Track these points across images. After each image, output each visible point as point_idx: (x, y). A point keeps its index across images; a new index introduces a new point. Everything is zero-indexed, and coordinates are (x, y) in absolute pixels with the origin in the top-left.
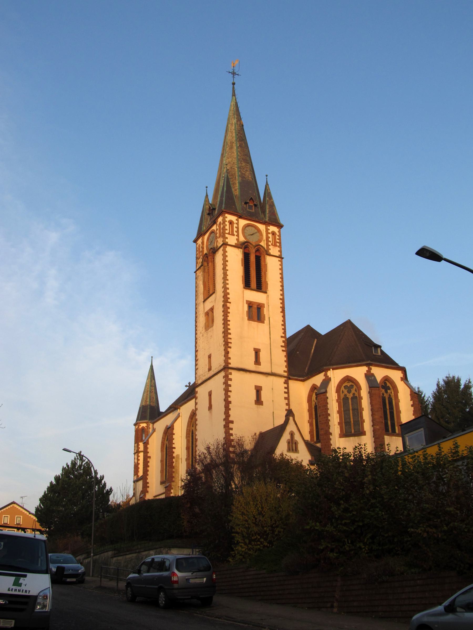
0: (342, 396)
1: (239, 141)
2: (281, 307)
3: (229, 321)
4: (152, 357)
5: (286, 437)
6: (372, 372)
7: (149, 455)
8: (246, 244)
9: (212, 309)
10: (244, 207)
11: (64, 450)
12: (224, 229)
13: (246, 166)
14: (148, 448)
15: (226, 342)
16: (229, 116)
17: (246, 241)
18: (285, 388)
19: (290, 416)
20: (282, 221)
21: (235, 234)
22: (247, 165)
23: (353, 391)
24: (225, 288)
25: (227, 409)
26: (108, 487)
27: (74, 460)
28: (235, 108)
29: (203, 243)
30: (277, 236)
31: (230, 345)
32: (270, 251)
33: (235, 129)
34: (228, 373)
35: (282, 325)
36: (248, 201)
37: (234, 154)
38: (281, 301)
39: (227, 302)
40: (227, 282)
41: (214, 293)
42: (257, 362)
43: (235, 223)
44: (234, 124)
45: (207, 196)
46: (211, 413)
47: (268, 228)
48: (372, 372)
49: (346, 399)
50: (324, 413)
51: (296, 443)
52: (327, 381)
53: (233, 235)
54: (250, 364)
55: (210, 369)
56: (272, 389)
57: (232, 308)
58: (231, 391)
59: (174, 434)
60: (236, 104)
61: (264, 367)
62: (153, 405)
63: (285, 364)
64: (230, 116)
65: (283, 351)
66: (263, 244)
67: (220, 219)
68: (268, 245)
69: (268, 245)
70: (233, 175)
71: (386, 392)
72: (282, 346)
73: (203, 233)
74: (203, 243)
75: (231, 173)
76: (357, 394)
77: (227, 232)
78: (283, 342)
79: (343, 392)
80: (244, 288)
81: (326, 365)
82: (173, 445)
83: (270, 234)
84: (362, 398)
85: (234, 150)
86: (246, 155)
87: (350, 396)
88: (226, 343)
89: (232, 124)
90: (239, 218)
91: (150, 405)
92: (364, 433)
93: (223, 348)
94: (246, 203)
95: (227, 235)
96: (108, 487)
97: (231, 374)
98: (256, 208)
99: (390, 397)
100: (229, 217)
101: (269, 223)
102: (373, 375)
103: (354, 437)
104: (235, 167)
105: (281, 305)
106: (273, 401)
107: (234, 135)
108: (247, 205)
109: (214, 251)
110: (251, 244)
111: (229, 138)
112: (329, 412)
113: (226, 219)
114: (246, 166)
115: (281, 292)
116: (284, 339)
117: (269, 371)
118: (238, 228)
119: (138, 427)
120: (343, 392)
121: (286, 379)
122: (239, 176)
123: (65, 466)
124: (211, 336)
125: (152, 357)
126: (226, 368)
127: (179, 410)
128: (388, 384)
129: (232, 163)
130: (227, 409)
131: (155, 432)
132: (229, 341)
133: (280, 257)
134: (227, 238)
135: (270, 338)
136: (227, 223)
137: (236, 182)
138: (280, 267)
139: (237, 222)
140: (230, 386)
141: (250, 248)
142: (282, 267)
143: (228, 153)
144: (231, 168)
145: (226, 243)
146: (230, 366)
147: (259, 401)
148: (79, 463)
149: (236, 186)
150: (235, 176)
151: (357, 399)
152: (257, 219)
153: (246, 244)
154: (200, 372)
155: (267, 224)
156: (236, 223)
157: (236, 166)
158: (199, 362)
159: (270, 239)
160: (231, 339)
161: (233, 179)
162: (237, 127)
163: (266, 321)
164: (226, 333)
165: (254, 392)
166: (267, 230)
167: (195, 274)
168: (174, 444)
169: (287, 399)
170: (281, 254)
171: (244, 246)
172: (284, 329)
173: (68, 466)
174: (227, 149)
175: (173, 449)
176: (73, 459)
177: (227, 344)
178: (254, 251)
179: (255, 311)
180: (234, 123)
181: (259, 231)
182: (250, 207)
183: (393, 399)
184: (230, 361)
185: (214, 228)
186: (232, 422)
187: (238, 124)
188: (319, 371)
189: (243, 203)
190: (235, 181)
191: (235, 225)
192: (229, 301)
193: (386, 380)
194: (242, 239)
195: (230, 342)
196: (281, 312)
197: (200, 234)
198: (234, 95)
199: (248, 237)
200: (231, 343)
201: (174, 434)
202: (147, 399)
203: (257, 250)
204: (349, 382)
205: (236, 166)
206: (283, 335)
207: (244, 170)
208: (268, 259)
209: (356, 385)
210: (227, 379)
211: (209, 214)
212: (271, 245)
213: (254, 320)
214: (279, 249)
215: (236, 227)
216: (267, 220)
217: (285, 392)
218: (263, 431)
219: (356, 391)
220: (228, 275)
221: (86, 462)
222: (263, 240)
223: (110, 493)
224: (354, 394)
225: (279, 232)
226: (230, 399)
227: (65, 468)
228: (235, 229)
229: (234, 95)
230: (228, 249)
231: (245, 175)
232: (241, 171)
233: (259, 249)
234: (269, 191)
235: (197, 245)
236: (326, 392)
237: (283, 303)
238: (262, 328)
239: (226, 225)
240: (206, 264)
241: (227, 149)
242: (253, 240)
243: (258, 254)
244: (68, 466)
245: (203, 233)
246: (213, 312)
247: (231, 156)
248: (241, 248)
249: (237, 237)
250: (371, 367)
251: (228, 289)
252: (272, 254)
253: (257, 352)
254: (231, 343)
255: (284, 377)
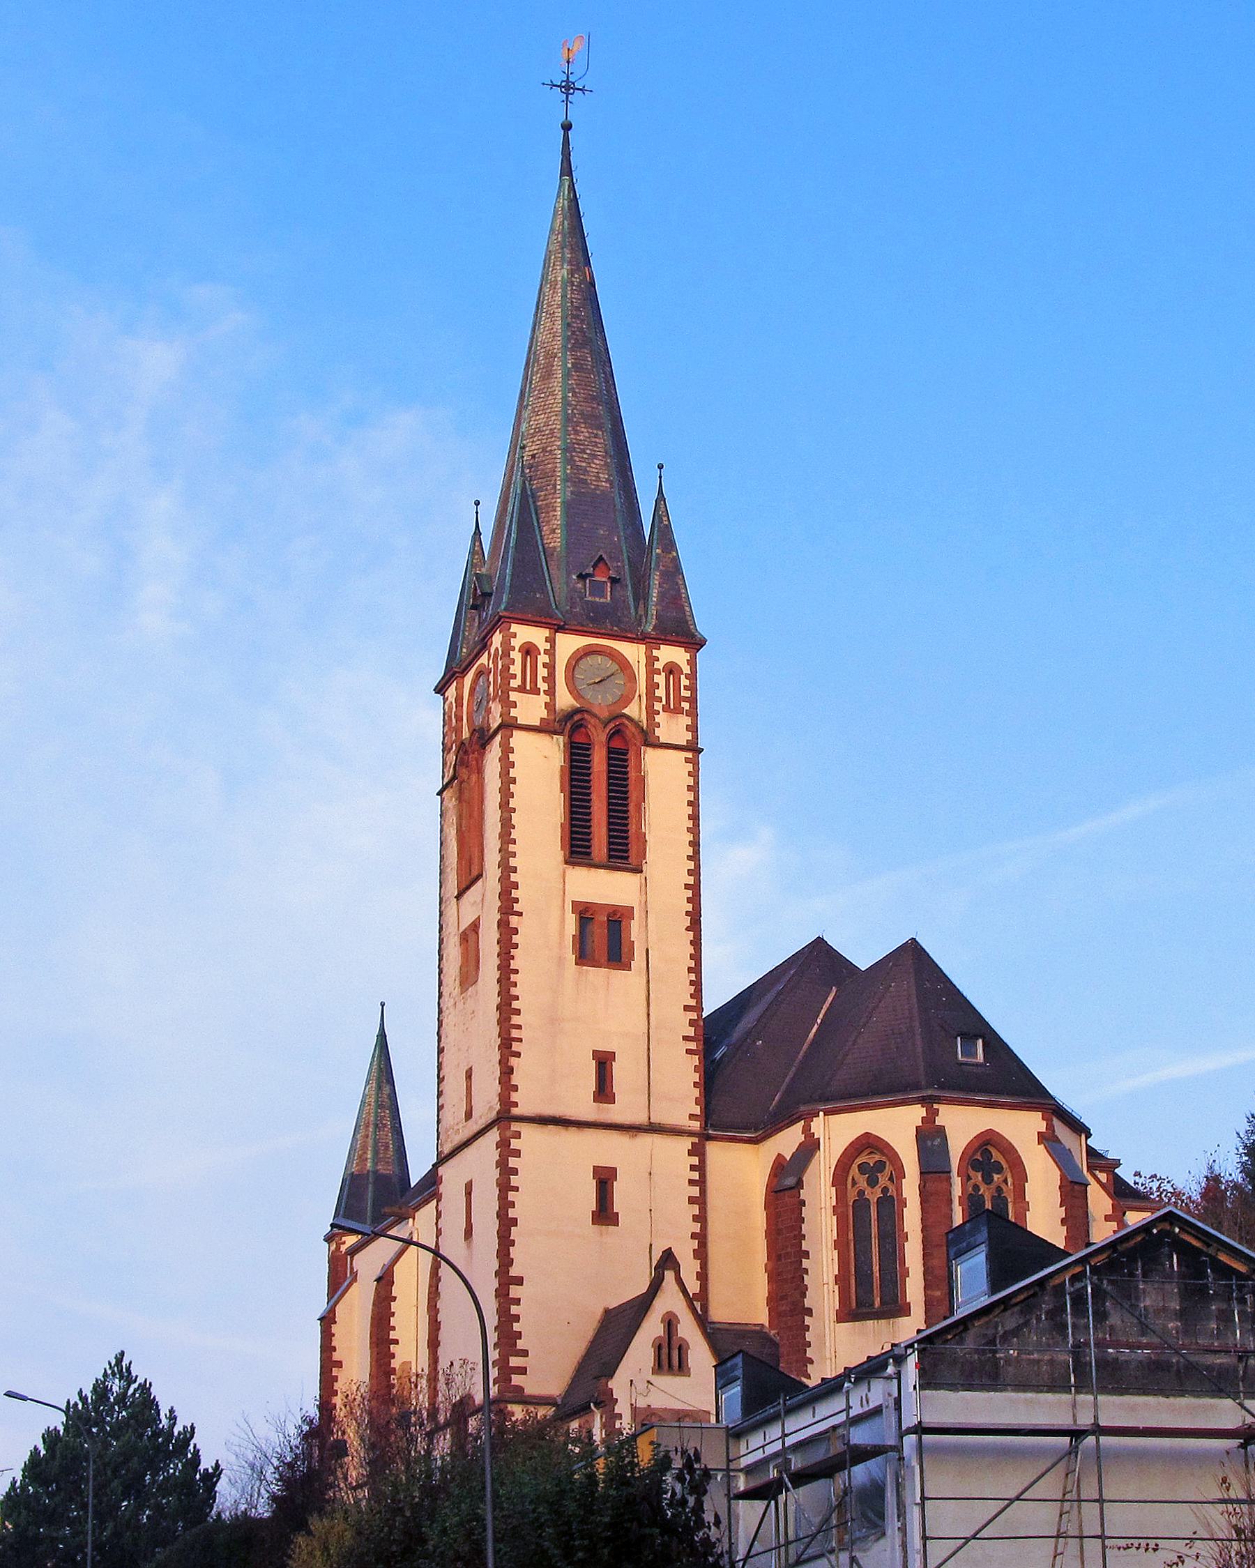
0: (852, 1195)
1: (571, 350)
2: (687, 913)
3: (517, 972)
4: (383, 1005)
5: (652, 1328)
6: (939, 1121)
7: (336, 1356)
8: (576, 718)
9: (475, 926)
10: (574, 590)
11: (9, 1394)
12: (507, 676)
13: (593, 440)
14: (334, 1335)
15: (505, 1039)
16: (549, 253)
17: (579, 706)
18: (693, 1168)
19: (667, 1269)
20: (702, 626)
21: (543, 686)
22: (596, 436)
23: (883, 1180)
24: (507, 869)
25: (505, 1242)
26: (206, 1464)
27: (102, 1379)
28: (566, 222)
29: (459, 699)
30: (683, 677)
31: (515, 1047)
32: (658, 732)
33: (561, 306)
34: (508, 1134)
35: (690, 970)
36: (590, 570)
37: (555, 399)
38: (690, 893)
39: (510, 911)
40: (512, 848)
41: (480, 876)
42: (604, 1092)
43: (542, 652)
44: (559, 286)
45: (477, 533)
46: (469, 1246)
47: (655, 653)
48: (939, 1121)
49: (861, 1204)
50: (789, 1250)
51: (683, 1349)
52: (810, 1147)
53: (535, 691)
54: (582, 1104)
55: (469, 1115)
56: (650, 1174)
57: (526, 930)
58: (516, 1189)
59: (394, 1299)
60: (574, 201)
61: (626, 1108)
62: (384, 1172)
63: (696, 1092)
64: (550, 251)
65: (689, 1052)
66: (635, 710)
67: (497, 639)
68: (652, 713)
69: (652, 713)
70: (548, 476)
71: (988, 1180)
72: (685, 1038)
73: (459, 670)
74: (459, 699)
75: (543, 470)
76: (892, 1191)
77: (515, 683)
78: (692, 1023)
79: (854, 1183)
80: (567, 863)
81: (811, 1100)
82: (391, 1332)
83: (660, 674)
84: (904, 1203)
85: (555, 384)
86: (593, 398)
87: (874, 1195)
88: (505, 1041)
89: (553, 285)
90: (557, 631)
91: (375, 1172)
92: (905, 1310)
93: (496, 1056)
94: (582, 577)
95: (514, 696)
96: (206, 1464)
97: (518, 1135)
98: (619, 588)
99: (999, 1195)
100: (525, 634)
101: (658, 637)
102: (941, 1131)
103: (876, 1321)
104: (553, 448)
105: (690, 907)
106: (651, 1210)
107: (558, 326)
108: (588, 581)
109: (482, 738)
110: (595, 716)
111: (542, 337)
112: (805, 1246)
113: (514, 642)
114: (593, 440)
115: (691, 865)
116: (694, 1016)
117: (640, 1118)
118: (551, 667)
119: (338, 1248)
120: (854, 1183)
121: (696, 1140)
122: (567, 479)
123: (75, 1398)
124: (473, 1012)
125: (383, 1005)
126: (505, 1118)
127: (411, 1220)
128: (996, 1156)
129: (547, 432)
130: (505, 1242)
131: (356, 1282)
132: (515, 1033)
133: (693, 748)
134: (514, 705)
135: (648, 1015)
136: (516, 655)
137: (555, 502)
138: (691, 781)
139: (548, 646)
140: (515, 1172)
141: (593, 730)
142: (697, 783)
143: (536, 392)
144: (544, 450)
145: (513, 722)
146: (515, 1111)
147: (605, 1214)
148: (116, 1386)
149: (554, 515)
150: (554, 478)
151: (891, 1206)
152: (615, 628)
153: (576, 718)
154: (449, 1117)
155: (651, 641)
156: (546, 652)
157: (559, 443)
158: (446, 1086)
159: (661, 692)
160: (519, 1027)
161: (547, 490)
162: (569, 296)
163: (638, 962)
164: (506, 1008)
165: (593, 1184)
166: (651, 660)
167: (439, 797)
168: (394, 1328)
169: (700, 1201)
170: (695, 737)
171: (569, 725)
172: (697, 985)
173: (83, 1399)
174: (534, 378)
175: (392, 1346)
176: (99, 1378)
177: (507, 1046)
178: (603, 737)
179: (599, 933)
180: (559, 279)
181: (624, 665)
182: (598, 589)
183: (1009, 1200)
184: (515, 1097)
185: (484, 659)
186: (519, 1281)
187: (572, 284)
188: (790, 1117)
189: (574, 577)
190: (552, 499)
191: (543, 659)
192: (516, 907)
193: (988, 1143)
194: (565, 700)
195: (519, 1038)
196: (688, 929)
197: (453, 673)
198: (567, 170)
199: (589, 695)
200: (520, 1040)
201: (394, 1299)
202: (365, 1153)
203: (617, 732)
204: (872, 1153)
205: (559, 443)
206: (693, 1003)
207: (585, 456)
208: (651, 757)
209: (892, 1164)
210: (506, 1150)
211: (474, 607)
212: (661, 711)
213: (596, 964)
214: (688, 721)
215: (545, 665)
216: (649, 629)
217: (692, 1182)
218: (613, 1304)
219: (891, 1179)
220: (514, 827)
221: (140, 1384)
222: (637, 694)
223: (215, 1479)
224: (885, 1190)
225: (692, 663)
226: (512, 1213)
227: (76, 1404)
228: (542, 672)
229: (567, 170)
230: (519, 740)
231: (586, 471)
232: (575, 461)
233: (621, 727)
234: (666, 523)
235: (445, 700)
236: (799, 1184)
237: (695, 900)
238: (627, 982)
239: (513, 662)
240: (464, 773)
241: (536, 378)
242: (601, 701)
243: (617, 744)
244: (83, 1399)
245: (460, 668)
246: (477, 933)
247: (545, 405)
248: (561, 734)
249: (547, 699)
250: (935, 1106)
251: (515, 870)
252: (662, 740)
253: (604, 1062)
254: (520, 1040)
255: (691, 1134)
